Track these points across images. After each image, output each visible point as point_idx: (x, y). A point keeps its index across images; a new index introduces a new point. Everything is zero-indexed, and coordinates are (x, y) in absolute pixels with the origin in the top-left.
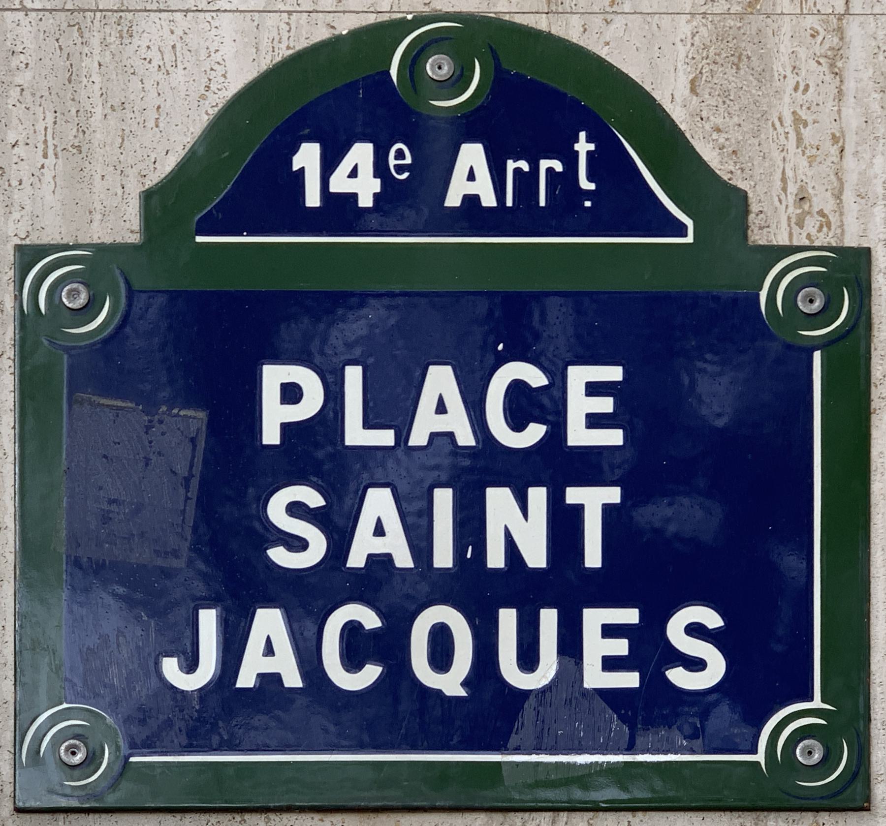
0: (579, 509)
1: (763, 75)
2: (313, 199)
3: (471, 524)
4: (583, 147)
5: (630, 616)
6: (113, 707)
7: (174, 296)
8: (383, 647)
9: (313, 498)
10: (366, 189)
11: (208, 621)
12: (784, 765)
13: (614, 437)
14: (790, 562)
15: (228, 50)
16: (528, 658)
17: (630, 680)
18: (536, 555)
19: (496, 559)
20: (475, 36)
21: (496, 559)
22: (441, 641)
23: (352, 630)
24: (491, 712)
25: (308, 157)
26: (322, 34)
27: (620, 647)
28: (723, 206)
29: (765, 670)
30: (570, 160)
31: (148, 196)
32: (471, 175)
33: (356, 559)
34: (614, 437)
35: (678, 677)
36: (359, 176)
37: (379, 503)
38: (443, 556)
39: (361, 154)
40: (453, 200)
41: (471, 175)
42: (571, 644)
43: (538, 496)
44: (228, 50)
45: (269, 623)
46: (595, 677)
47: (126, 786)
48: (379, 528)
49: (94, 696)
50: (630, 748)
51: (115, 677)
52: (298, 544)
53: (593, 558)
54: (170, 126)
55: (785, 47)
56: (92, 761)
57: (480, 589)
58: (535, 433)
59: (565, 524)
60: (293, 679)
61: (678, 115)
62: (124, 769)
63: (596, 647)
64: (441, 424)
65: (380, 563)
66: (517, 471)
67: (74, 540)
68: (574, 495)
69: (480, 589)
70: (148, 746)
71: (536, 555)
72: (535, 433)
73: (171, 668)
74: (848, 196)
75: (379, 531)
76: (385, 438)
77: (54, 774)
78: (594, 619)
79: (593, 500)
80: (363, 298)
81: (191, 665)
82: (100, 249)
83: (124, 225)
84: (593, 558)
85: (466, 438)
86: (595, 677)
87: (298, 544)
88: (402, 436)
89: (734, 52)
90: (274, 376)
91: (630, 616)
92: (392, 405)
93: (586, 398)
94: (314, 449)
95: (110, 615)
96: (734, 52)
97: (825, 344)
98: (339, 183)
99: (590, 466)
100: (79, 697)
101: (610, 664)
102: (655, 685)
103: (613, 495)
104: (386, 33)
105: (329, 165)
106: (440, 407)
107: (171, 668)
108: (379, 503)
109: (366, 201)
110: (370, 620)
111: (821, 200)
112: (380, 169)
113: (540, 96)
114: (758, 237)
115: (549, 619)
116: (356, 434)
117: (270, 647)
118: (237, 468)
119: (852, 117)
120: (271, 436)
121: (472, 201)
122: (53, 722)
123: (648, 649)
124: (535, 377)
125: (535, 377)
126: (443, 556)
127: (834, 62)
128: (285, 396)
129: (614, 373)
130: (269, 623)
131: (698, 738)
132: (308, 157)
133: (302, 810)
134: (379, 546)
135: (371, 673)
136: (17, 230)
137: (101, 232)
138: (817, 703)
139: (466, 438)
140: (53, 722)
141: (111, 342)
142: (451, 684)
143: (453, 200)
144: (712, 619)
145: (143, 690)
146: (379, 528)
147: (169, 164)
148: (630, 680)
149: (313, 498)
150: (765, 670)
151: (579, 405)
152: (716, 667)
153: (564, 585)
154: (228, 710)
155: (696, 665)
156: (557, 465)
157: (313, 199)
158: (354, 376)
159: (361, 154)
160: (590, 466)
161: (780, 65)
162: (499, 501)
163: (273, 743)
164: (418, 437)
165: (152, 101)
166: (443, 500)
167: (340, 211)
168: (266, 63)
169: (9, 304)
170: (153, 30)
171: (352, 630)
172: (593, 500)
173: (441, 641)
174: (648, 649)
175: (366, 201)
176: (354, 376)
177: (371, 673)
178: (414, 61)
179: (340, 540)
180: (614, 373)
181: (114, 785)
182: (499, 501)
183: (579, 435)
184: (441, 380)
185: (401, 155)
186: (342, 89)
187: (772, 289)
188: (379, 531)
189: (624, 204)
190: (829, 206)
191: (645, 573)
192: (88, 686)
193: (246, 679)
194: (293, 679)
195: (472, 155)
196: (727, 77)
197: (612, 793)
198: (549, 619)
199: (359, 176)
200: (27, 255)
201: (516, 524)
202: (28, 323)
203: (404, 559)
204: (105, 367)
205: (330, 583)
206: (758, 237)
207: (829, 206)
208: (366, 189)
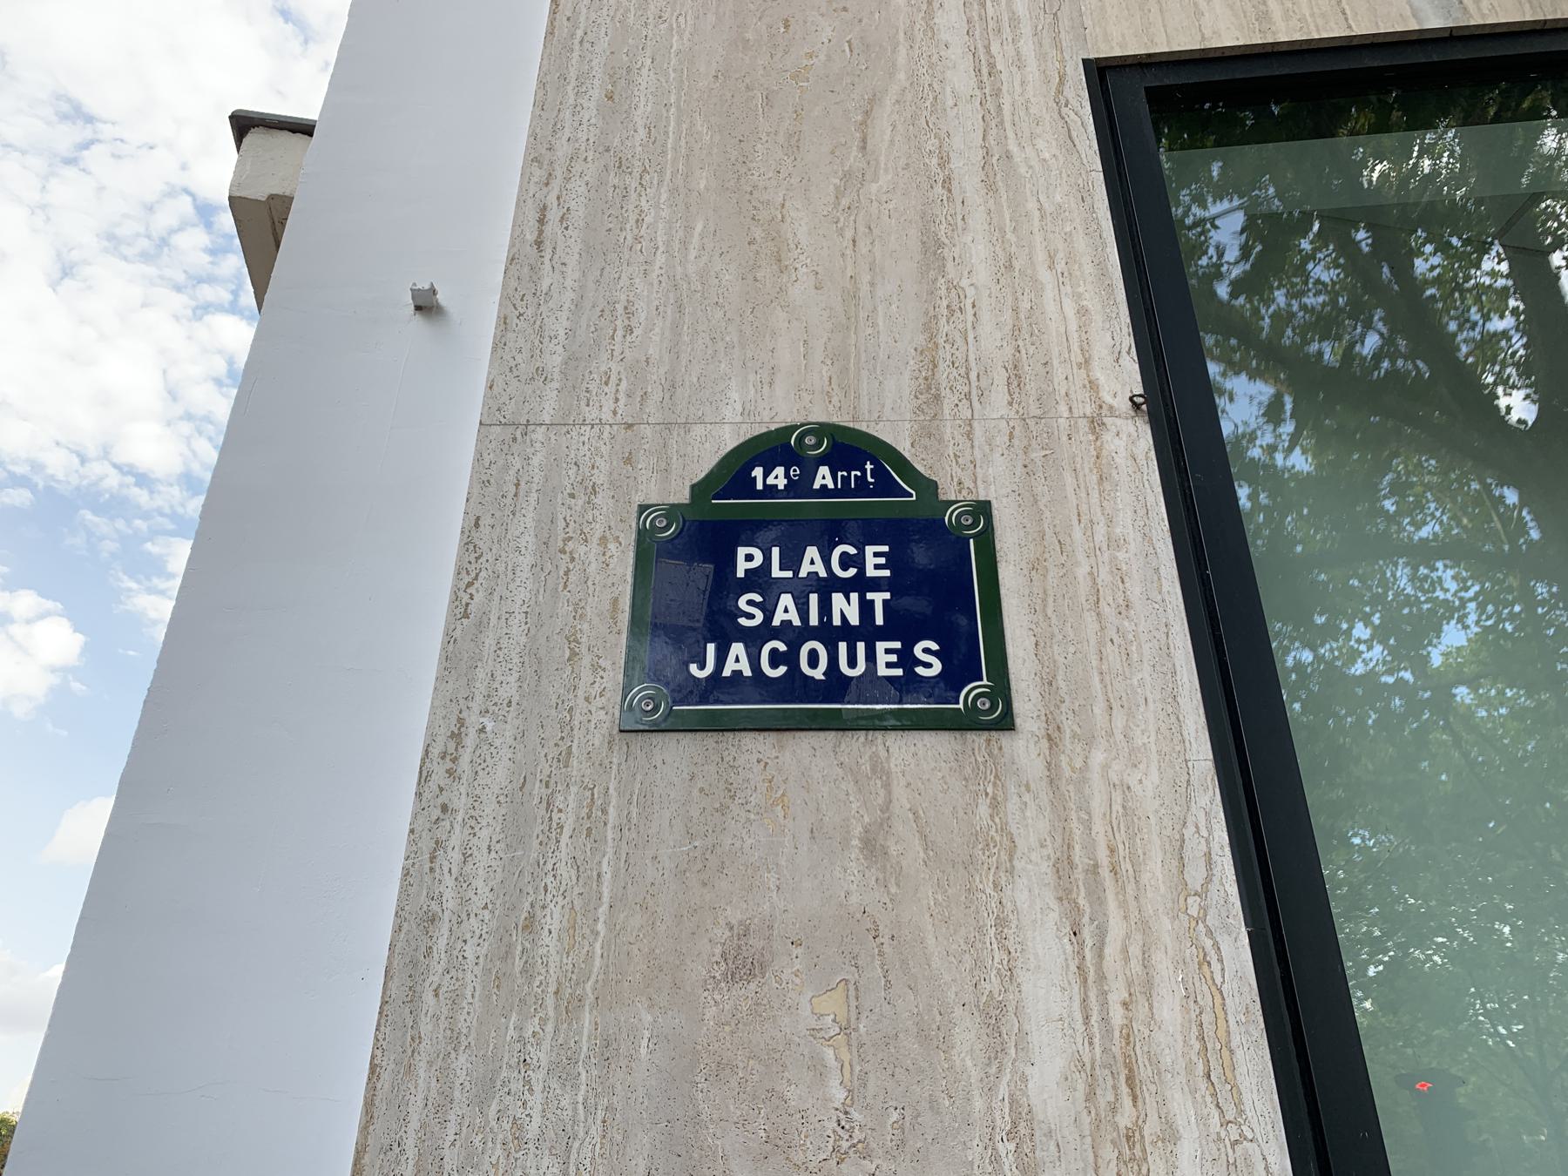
0: (872, 602)
1: (941, 441)
2: (760, 486)
3: (825, 607)
4: (869, 466)
5: (897, 645)
6: (667, 684)
7: (702, 523)
8: (790, 658)
9: (758, 598)
10: (781, 483)
11: (711, 648)
12: (972, 709)
13: (887, 573)
14: (963, 621)
15: (727, 436)
16: (852, 663)
17: (899, 672)
18: (854, 620)
19: (837, 621)
20: (822, 430)
21: (837, 621)
22: (813, 655)
23: (774, 651)
24: (837, 686)
25: (758, 472)
26: (764, 430)
27: (893, 658)
28: (928, 487)
29: (960, 669)
30: (864, 472)
31: (693, 487)
32: (823, 478)
33: (776, 622)
34: (887, 573)
35: (920, 670)
36: (778, 478)
37: (786, 600)
38: (814, 620)
39: (780, 471)
40: (816, 486)
41: (823, 478)
42: (871, 657)
43: (854, 596)
44: (727, 436)
45: (738, 649)
46: (882, 671)
47: (670, 720)
48: (786, 610)
49: (659, 681)
50: (900, 702)
51: (669, 673)
52: (751, 616)
53: (879, 621)
54: (704, 463)
55: (948, 431)
56: (656, 709)
57: (830, 634)
58: (852, 572)
59: (866, 608)
60: (747, 673)
61: (907, 455)
62: (670, 712)
63: (882, 658)
64: (812, 569)
65: (787, 624)
66: (846, 587)
67: (655, 616)
68: (869, 596)
69: (830, 634)
70: (681, 703)
71: (854, 620)
72: (852, 572)
73: (693, 668)
74: (979, 482)
75: (786, 611)
76: (789, 574)
77: (638, 714)
78: (881, 646)
79: (878, 598)
80: (770, 522)
81: (702, 667)
82: (673, 505)
83: (683, 496)
84: (879, 621)
85: (823, 574)
86: (882, 671)
87: (751, 616)
88: (796, 573)
89: (928, 433)
90: (742, 552)
91: (897, 645)
92: (792, 560)
93: (874, 560)
94: (759, 579)
95: (664, 649)
96: (928, 433)
97: (974, 536)
98: (770, 481)
99: (876, 585)
100: (652, 681)
101: (889, 665)
102: (910, 675)
103: (887, 596)
104: (791, 429)
105: (765, 476)
106: (812, 562)
107: (693, 668)
108: (786, 600)
109: (781, 487)
110: (782, 647)
111: (968, 483)
112: (787, 475)
113: (847, 448)
114: (942, 497)
115: (861, 646)
116: (776, 572)
117: (738, 659)
118: (725, 585)
119: (978, 454)
120: (740, 574)
121: (824, 487)
122: (639, 692)
123: (906, 659)
124: (852, 551)
125: (852, 551)
126: (814, 620)
127: (969, 435)
128: (746, 559)
129: (885, 549)
130: (738, 649)
131: (931, 698)
132: (758, 472)
133: (745, 730)
134: (786, 617)
135: (782, 670)
136: (639, 499)
137: (673, 500)
138: (985, 682)
139: (823, 574)
140: (639, 692)
141: (671, 540)
142: (818, 674)
143: (816, 486)
144: (934, 646)
145: (680, 678)
146: (786, 610)
147: (703, 475)
148: (899, 672)
149: (758, 598)
150: (960, 669)
151: (870, 561)
152: (937, 667)
153: (867, 632)
154: (718, 686)
155: (928, 665)
156: (862, 584)
157: (760, 486)
158: (776, 551)
159: (780, 471)
160: (876, 585)
161: (947, 436)
162: (838, 599)
163: (722, 697)
164: (803, 574)
165: (696, 453)
166: (814, 599)
167: (770, 491)
168: (742, 440)
169: (634, 525)
170: (698, 430)
171: (774, 651)
172: (878, 598)
173: (813, 655)
174: (906, 659)
175: (781, 487)
176: (776, 551)
177: (782, 670)
178: (800, 439)
179: (769, 615)
180: (885, 549)
181: (665, 720)
182: (838, 599)
183: (871, 572)
184: (812, 552)
185: (795, 471)
186: (774, 448)
187: (950, 517)
188: (786, 611)
189: (885, 485)
190: (972, 486)
191: (903, 627)
192: (655, 676)
193: (727, 673)
194: (747, 673)
195: (824, 470)
196: (925, 441)
197: (893, 722)
198: (861, 646)
199: (778, 478)
200: (643, 508)
201: (846, 608)
202: (642, 534)
203: (797, 622)
204: (669, 550)
205: (767, 631)
206: (942, 497)
207: (972, 486)
208: (781, 483)
